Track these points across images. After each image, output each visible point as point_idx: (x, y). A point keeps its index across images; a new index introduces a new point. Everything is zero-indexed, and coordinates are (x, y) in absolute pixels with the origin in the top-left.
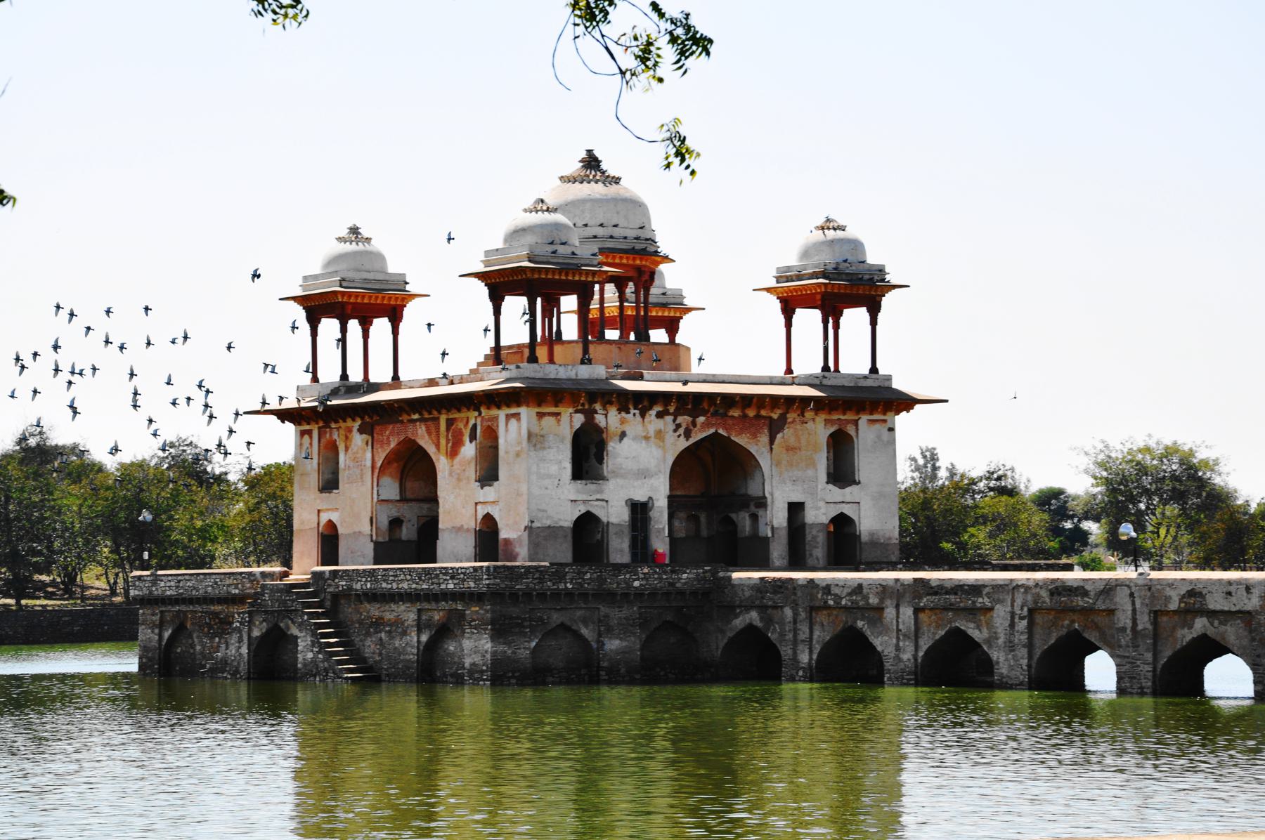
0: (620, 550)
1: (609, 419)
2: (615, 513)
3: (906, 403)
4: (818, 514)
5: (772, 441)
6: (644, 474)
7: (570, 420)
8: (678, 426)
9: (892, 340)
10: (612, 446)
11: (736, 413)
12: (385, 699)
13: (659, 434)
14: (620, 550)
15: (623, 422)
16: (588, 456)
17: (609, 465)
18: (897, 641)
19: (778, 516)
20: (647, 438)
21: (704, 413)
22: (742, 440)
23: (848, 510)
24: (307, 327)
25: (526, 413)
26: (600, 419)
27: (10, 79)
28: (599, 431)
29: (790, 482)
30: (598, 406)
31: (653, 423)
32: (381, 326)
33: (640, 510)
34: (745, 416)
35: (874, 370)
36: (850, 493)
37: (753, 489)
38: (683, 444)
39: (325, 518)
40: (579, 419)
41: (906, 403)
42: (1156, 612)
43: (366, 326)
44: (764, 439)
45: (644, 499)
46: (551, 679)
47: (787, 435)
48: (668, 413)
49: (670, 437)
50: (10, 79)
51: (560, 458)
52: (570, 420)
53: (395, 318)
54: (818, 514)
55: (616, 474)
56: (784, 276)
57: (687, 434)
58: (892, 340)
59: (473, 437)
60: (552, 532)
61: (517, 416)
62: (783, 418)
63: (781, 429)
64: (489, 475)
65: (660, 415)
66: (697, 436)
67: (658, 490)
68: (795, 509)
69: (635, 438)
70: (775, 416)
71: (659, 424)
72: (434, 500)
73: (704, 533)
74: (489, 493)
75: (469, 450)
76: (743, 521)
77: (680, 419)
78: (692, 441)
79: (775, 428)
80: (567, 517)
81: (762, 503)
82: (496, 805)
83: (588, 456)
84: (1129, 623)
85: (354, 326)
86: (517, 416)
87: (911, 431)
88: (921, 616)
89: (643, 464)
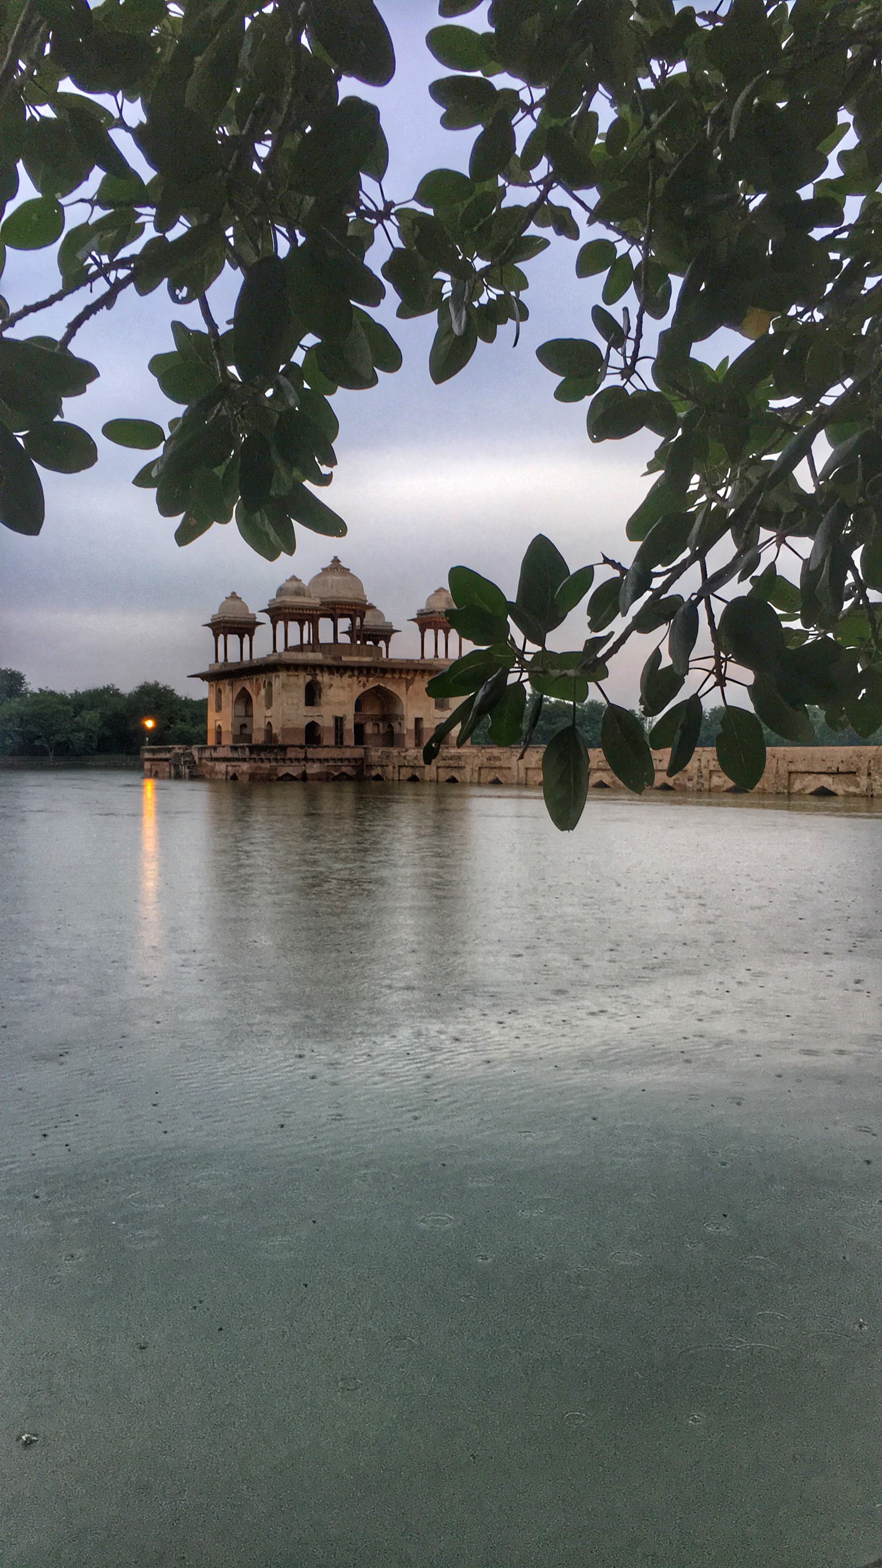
0: (329, 739)
1: (324, 679)
2: (326, 722)
5: (407, 690)
7: (303, 679)
8: (360, 682)
10: (325, 691)
11: (389, 676)
12: (844, 967)
13: (350, 685)
14: (329, 739)
15: (331, 679)
16: (312, 695)
17: (324, 699)
19: (410, 725)
20: (343, 688)
21: (373, 676)
22: (391, 688)
23: (317, 720)
24: (271, 625)
25: (283, 675)
26: (319, 678)
27: (515, 345)
28: (318, 683)
30: (318, 672)
31: (346, 680)
33: (339, 721)
34: (393, 678)
35: (423, 657)
37: (398, 712)
38: (362, 690)
39: (218, 723)
40: (309, 678)
42: (527, 769)
45: (341, 715)
46: (402, 825)
48: (353, 675)
49: (355, 687)
50: (515, 345)
51: (300, 695)
52: (303, 679)
53: (251, 634)
55: (327, 704)
56: (421, 614)
57: (364, 685)
59: (264, 687)
60: (295, 730)
61: (278, 676)
62: (413, 679)
63: (412, 684)
64: (269, 705)
65: (350, 677)
66: (369, 686)
68: (418, 721)
69: (338, 687)
70: (409, 678)
71: (350, 680)
73: (381, 731)
74: (269, 713)
75: (263, 692)
76: (395, 725)
77: (361, 679)
78: (367, 689)
80: (303, 723)
81: (402, 718)
83: (312, 695)
84: (516, 774)
85: (441, 632)
86: (278, 676)
88: (440, 770)
89: (340, 697)
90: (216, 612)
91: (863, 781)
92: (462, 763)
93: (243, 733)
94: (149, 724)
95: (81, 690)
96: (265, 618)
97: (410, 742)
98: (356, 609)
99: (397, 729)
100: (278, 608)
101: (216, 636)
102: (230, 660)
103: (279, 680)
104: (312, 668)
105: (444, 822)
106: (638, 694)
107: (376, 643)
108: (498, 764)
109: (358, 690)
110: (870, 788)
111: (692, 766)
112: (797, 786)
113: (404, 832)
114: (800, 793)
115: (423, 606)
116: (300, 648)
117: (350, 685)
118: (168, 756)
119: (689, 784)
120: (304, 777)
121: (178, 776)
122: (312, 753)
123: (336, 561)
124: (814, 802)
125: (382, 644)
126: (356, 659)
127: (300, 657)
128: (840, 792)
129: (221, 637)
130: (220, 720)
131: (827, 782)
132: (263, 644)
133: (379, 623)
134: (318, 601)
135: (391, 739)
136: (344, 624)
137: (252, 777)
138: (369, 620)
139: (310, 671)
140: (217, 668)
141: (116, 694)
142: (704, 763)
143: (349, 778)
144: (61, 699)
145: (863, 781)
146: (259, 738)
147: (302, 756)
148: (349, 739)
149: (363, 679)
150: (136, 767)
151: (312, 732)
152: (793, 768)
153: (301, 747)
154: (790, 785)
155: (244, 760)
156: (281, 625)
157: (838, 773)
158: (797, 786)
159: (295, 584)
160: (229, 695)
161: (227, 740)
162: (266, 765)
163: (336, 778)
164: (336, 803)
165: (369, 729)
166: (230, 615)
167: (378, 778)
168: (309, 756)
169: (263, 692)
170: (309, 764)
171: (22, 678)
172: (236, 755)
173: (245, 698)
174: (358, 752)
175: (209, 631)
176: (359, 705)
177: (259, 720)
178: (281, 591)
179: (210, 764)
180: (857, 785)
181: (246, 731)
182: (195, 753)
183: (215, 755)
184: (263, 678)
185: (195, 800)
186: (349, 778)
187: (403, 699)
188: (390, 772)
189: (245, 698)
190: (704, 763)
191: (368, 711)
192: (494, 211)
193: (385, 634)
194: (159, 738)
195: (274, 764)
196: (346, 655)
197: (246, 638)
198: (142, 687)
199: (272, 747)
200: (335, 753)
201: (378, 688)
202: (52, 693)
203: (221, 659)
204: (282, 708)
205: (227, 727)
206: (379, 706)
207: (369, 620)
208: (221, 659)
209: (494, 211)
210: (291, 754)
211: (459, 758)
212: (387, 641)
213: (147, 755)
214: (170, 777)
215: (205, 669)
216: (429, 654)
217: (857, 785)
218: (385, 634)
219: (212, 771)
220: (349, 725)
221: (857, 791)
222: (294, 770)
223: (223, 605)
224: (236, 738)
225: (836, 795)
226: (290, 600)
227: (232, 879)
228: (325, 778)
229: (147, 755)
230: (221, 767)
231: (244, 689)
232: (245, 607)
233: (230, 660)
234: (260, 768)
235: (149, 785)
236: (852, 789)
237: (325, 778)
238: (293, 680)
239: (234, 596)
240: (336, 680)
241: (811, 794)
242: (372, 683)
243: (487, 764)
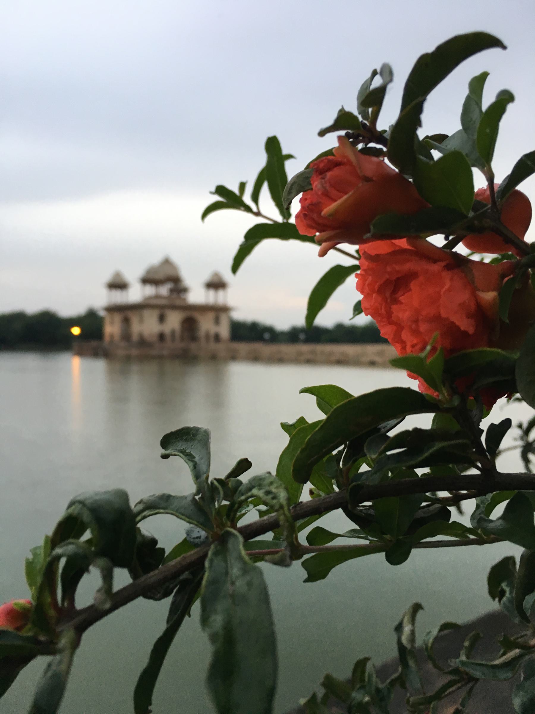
16: (162, 319)
29: (206, 325)
83: (162, 319)
89: (174, 321)
93: (126, 336)
95: (430, 48)
105: (218, 381)
106: (459, 252)
111: (386, 337)
139: (161, 309)
146: (135, 338)
151: (161, 337)
173: (126, 321)
185: (100, 365)
189: (126, 321)
192: (505, 261)
199: (143, 342)
204: (148, 326)
206: (190, 325)
209: (505, 261)
227: (118, 399)
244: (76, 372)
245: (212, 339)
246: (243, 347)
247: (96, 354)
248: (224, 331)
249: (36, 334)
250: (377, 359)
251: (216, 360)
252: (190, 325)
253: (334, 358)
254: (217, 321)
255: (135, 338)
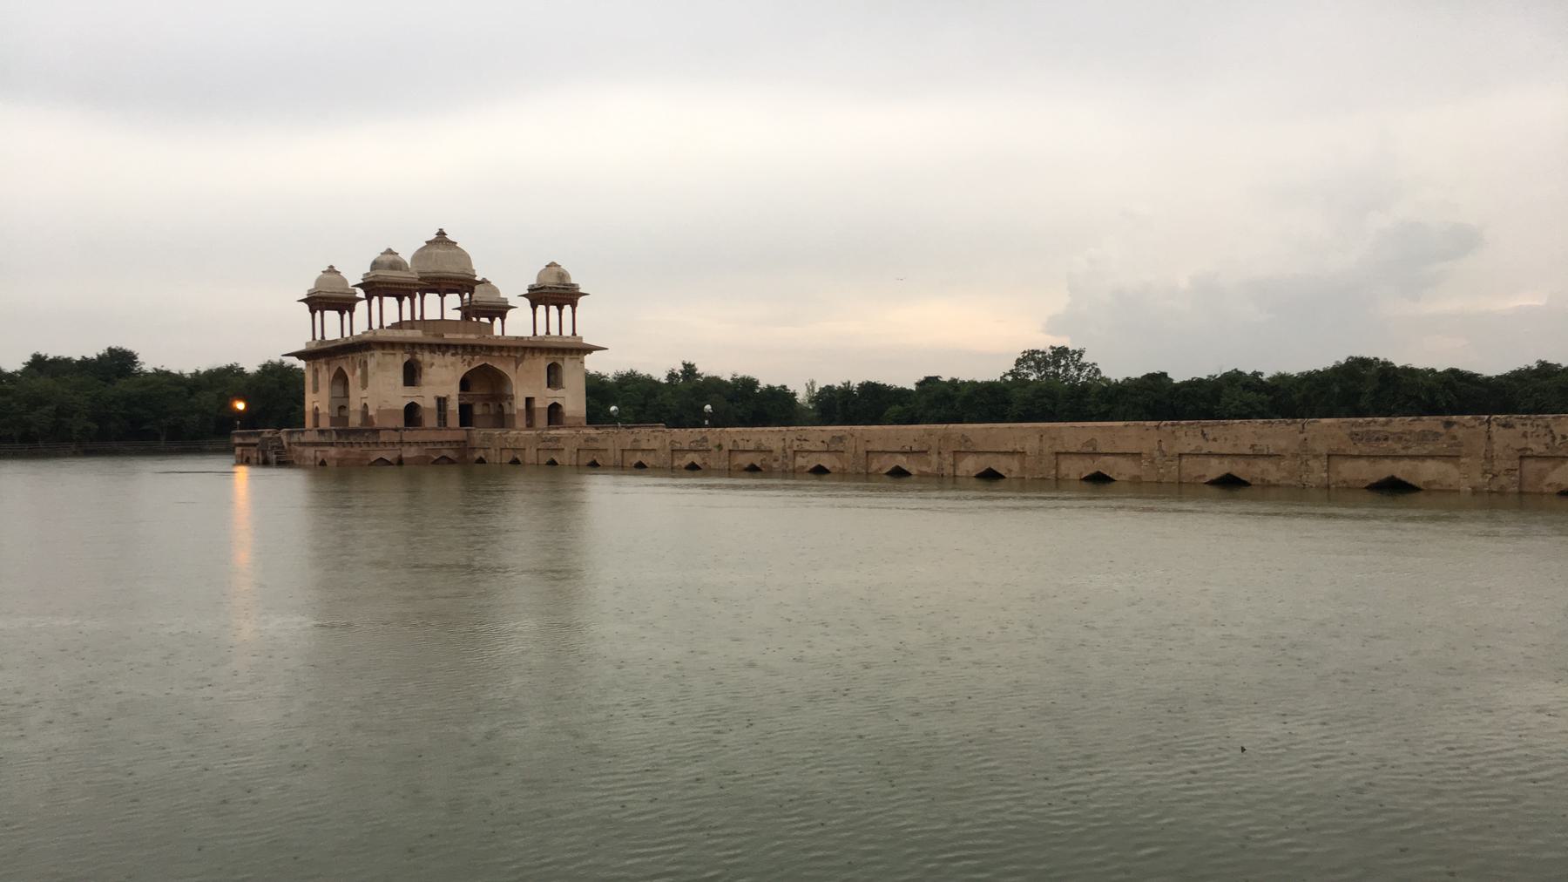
0: (430, 421)
1: (425, 357)
3: (589, 349)
4: (541, 404)
6: (443, 383)
7: (400, 359)
9: (587, 322)
10: (426, 370)
14: (430, 421)
16: (412, 375)
17: (424, 379)
18: (530, 455)
19: (520, 404)
22: (499, 366)
23: (417, 401)
25: (378, 354)
26: (419, 357)
28: (418, 362)
29: (526, 384)
31: (449, 358)
32: (567, 309)
33: (442, 402)
36: (559, 393)
40: (407, 357)
41: (589, 349)
43: (560, 308)
44: (513, 366)
47: (525, 364)
49: (460, 365)
52: (400, 359)
53: (352, 311)
54: (541, 404)
55: (429, 384)
58: (587, 322)
62: (523, 358)
64: (364, 385)
67: (453, 392)
68: (529, 401)
72: (347, 396)
74: (364, 394)
75: (358, 372)
76: (505, 404)
79: (518, 362)
80: (401, 404)
81: (512, 397)
82: (505, 569)
83: (412, 375)
85: (553, 309)
87: (592, 364)
89: (443, 379)
90: (312, 286)
91: (934, 458)
92: (560, 445)
94: (240, 406)
95: (203, 370)
96: (360, 293)
97: (521, 422)
98: (463, 283)
99: (507, 411)
100: (372, 283)
101: (313, 312)
102: (328, 338)
103: (374, 359)
104: (413, 346)
105: (562, 506)
107: (492, 320)
108: (595, 445)
109: (462, 369)
110: (941, 467)
112: (875, 466)
113: (519, 518)
114: (876, 473)
115: (534, 282)
116: (400, 325)
117: (453, 364)
118: (256, 440)
119: (775, 465)
120: (400, 462)
121: (266, 463)
122: (409, 436)
123: (441, 233)
124: (889, 482)
125: (498, 321)
126: (460, 336)
127: (398, 335)
128: (914, 471)
129: (417, 317)
130: (317, 400)
131: (902, 461)
132: (361, 321)
133: (494, 298)
134: (416, 276)
135: (502, 419)
136: (453, 300)
137: (341, 462)
138: (480, 294)
139: (412, 351)
140: (314, 346)
141: (241, 372)
142: (788, 442)
143: (451, 462)
144: (177, 379)
145: (934, 458)
146: (355, 421)
147: (397, 439)
148: (454, 420)
149: (468, 358)
150: (228, 450)
151: (412, 414)
152: (870, 448)
153: (396, 430)
154: (867, 466)
155: (331, 444)
156: (376, 300)
157: (911, 452)
158: (875, 466)
159: (391, 257)
160: (325, 376)
161: (325, 424)
162: (357, 449)
163: (435, 462)
164: (444, 489)
165: (478, 410)
166: (326, 290)
167: (481, 461)
168: (405, 439)
169: (358, 372)
170: (406, 448)
171: (135, 357)
172: (323, 440)
173: (341, 378)
174: (460, 435)
175: (305, 307)
176: (465, 384)
177: (355, 404)
178: (375, 265)
179: (300, 449)
180: (929, 464)
181: (343, 413)
182: (284, 438)
183: (303, 439)
184: (358, 356)
185: (290, 486)
186: (451, 462)
187: (512, 377)
188: (493, 456)
189: (341, 378)
190: (788, 442)
191: (477, 390)
193: (500, 310)
194: (249, 421)
195: (365, 448)
196: (449, 332)
197: (347, 315)
198: (265, 366)
199: (369, 430)
200: (433, 436)
201: (485, 368)
202: (168, 373)
203: (318, 337)
204: (381, 390)
205: (324, 409)
206: (484, 390)
207: (480, 294)
208: (318, 337)
210: (383, 437)
211: (558, 439)
212: (503, 318)
213: (238, 440)
214: (258, 464)
215: (302, 347)
216: (541, 332)
217: (929, 464)
218: (500, 310)
219: (301, 457)
220: (453, 406)
221: (929, 470)
222: (389, 455)
223: (319, 281)
224: (333, 421)
225: (1002, 477)
226: (384, 274)
228: (423, 461)
229: (238, 440)
230: (310, 452)
231: (340, 369)
232: (345, 281)
233: (328, 338)
234: (348, 453)
235: (243, 472)
236: (925, 469)
237: (423, 461)
238: (389, 358)
239: (331, 270)
240: (438, 359)
241: (1212, 483)
242: (478, 362)
243: (584, 445)
244: (242, 508)
245: (541, 420)
246: (615, 439)
247: (274, 458)
248: (574, 402)
249: (99, 410)
250: (826, 461)
251: (558, 470)
252: (484, 390)
253: (744, 460)
254: (554, 377)
255: (355, 421)
